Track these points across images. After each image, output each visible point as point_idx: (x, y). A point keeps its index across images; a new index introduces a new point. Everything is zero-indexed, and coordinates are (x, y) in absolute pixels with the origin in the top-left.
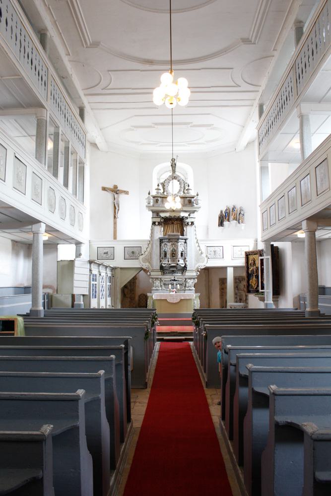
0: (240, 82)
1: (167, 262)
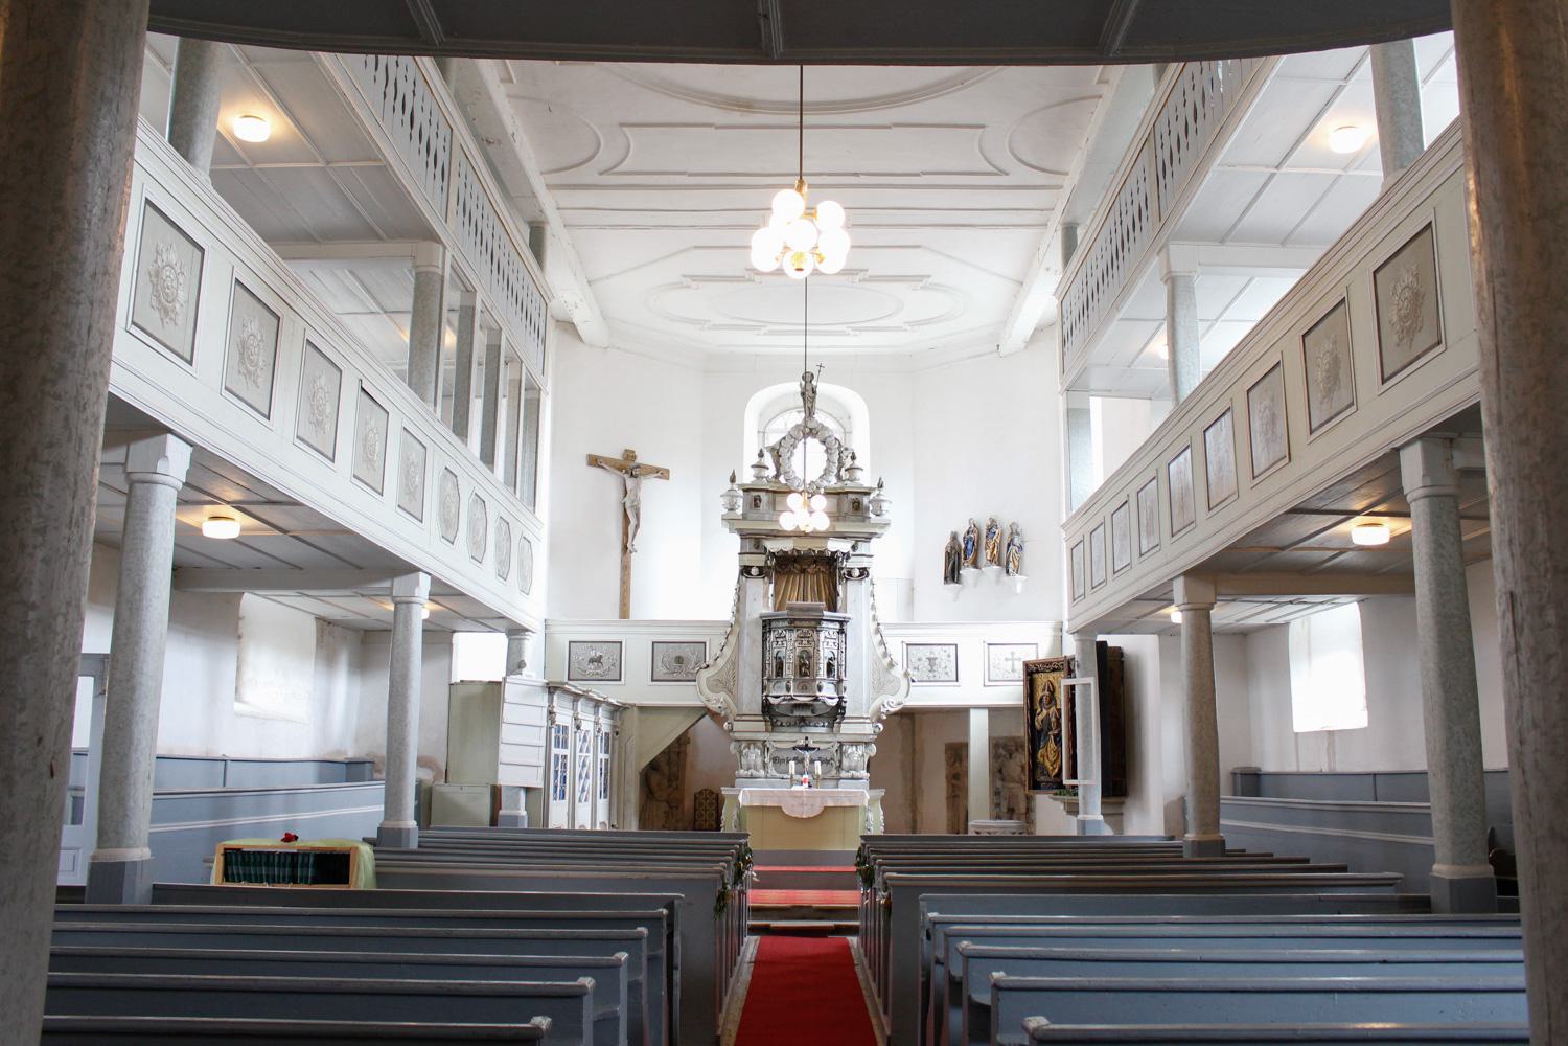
0: (1006, 161)
1: (784, 692)
